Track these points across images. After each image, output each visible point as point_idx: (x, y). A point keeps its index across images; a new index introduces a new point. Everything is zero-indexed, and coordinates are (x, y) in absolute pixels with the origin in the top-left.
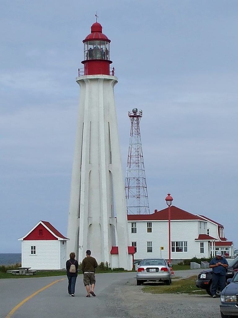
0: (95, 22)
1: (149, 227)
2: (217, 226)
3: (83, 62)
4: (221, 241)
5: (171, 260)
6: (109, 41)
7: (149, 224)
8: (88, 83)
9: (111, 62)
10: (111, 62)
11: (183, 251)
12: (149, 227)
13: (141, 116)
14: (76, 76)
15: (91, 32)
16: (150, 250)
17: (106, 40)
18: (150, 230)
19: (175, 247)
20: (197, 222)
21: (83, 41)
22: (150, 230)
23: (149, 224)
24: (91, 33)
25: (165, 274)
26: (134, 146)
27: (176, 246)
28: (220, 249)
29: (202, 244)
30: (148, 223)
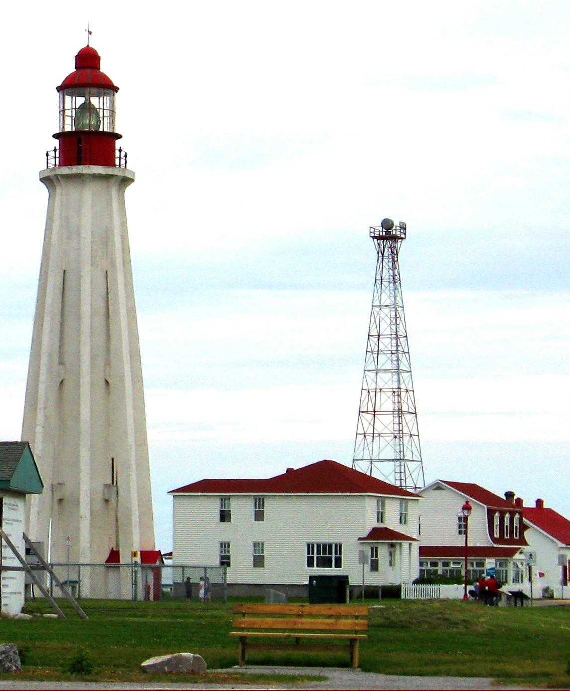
0: (84, 46)
1: (259, 508)
2: (486, 509)
3: (56, 136)
4: (495, 546)
5: (229, 584)
6: (116, 89)
7: (259, 503)
8: (61, 185)
9: (119, 136)
10: (119, 136)
11: (313, 567)
12: (259, 508)
13: (403, 236)
14: (40, 164)
15: (76, 68)
16: (259, 561)
17: (107, 87)
18: (259, 516)
19: (315, 556)
20: (399, 501)
21: (57, 88)
22: (259, 516)
23: (259, 503)
24: (75, 70)
25: (153, 613)
26: (386, 311)
27: (317, 554)
28: (440, 564)
29: (374, 552)
30: (256, 500)
